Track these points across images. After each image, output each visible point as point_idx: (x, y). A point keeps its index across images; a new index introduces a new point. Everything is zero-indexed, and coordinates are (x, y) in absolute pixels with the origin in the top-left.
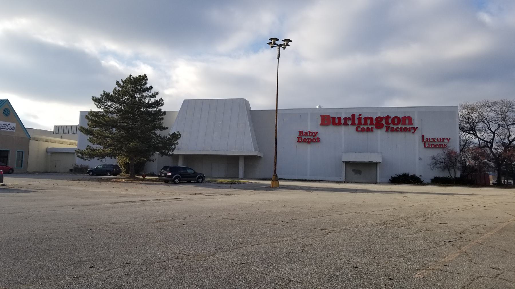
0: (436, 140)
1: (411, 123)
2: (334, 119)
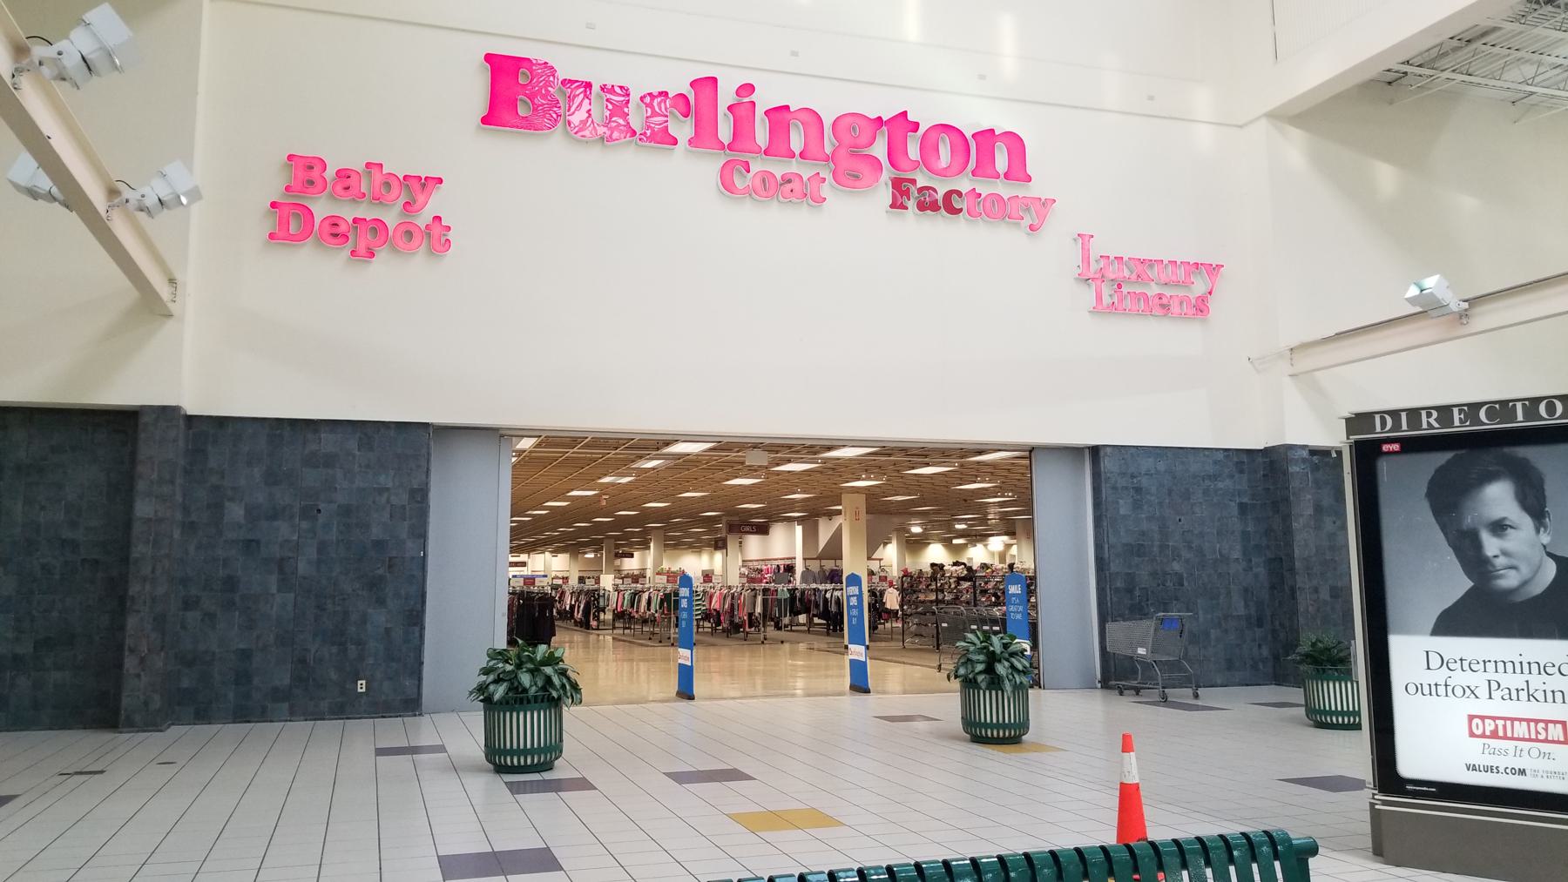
1: (1018, 172)
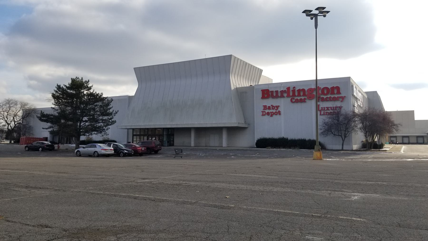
0: (330, 109)
1: (339, 93)
2: (272, 92)
